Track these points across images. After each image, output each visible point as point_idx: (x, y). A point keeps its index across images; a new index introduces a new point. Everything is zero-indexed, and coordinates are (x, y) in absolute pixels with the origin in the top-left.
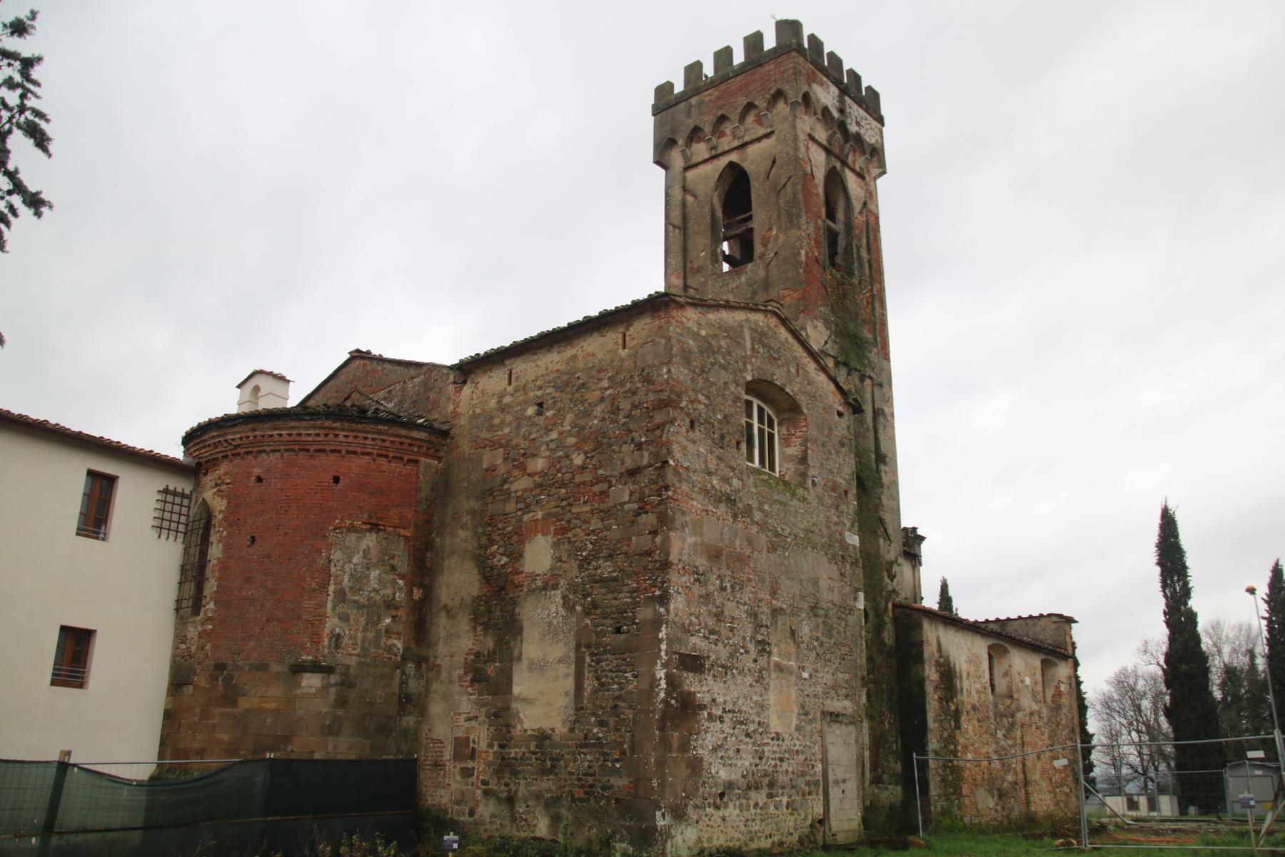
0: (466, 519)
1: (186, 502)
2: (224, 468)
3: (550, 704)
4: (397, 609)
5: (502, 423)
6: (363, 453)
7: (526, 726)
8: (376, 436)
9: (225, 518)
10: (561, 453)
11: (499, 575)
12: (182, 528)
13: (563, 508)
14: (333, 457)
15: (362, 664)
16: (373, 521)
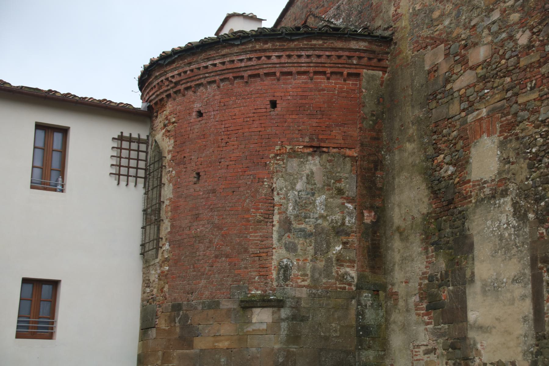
0: (412, 130)
1: (143, 147)
2: (170, 107)
3: (507, 332)
4: (348, 234)
5: (442, 15)
6: (299, 73)
7: (485, 359)
8: (310, 53)
9: (172, 159)
10: (504, 35)
11: (447, 187)
12: (141, 173)
13: (508, 99)
14: (268, 81)
15: (312, 296)
16: (315, 144)
